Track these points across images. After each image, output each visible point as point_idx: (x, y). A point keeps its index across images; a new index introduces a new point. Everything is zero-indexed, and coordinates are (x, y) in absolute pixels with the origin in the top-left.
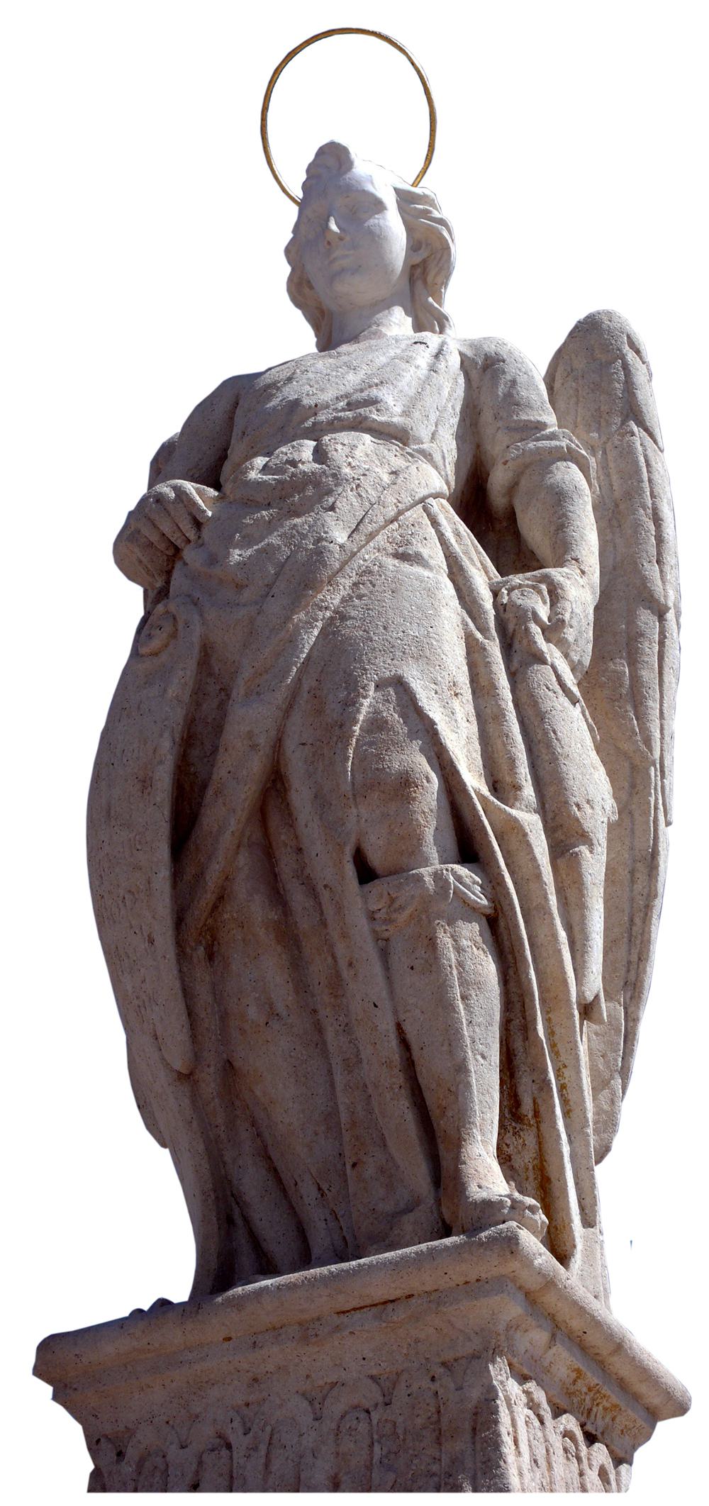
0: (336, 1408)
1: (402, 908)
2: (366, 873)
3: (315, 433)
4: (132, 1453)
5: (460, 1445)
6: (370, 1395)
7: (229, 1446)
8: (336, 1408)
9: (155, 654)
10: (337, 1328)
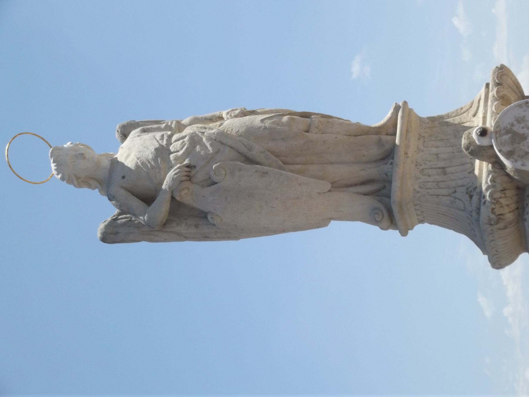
0: (421, 147)
1: (319, 126)
2: (307, 131)
3: (169, 143)
4: (418, 189)
5: (436, 123)
6: (422, 140)
7: (423, 169)
8: (421, 147)
9: (226, 174)
10: (409, 141)
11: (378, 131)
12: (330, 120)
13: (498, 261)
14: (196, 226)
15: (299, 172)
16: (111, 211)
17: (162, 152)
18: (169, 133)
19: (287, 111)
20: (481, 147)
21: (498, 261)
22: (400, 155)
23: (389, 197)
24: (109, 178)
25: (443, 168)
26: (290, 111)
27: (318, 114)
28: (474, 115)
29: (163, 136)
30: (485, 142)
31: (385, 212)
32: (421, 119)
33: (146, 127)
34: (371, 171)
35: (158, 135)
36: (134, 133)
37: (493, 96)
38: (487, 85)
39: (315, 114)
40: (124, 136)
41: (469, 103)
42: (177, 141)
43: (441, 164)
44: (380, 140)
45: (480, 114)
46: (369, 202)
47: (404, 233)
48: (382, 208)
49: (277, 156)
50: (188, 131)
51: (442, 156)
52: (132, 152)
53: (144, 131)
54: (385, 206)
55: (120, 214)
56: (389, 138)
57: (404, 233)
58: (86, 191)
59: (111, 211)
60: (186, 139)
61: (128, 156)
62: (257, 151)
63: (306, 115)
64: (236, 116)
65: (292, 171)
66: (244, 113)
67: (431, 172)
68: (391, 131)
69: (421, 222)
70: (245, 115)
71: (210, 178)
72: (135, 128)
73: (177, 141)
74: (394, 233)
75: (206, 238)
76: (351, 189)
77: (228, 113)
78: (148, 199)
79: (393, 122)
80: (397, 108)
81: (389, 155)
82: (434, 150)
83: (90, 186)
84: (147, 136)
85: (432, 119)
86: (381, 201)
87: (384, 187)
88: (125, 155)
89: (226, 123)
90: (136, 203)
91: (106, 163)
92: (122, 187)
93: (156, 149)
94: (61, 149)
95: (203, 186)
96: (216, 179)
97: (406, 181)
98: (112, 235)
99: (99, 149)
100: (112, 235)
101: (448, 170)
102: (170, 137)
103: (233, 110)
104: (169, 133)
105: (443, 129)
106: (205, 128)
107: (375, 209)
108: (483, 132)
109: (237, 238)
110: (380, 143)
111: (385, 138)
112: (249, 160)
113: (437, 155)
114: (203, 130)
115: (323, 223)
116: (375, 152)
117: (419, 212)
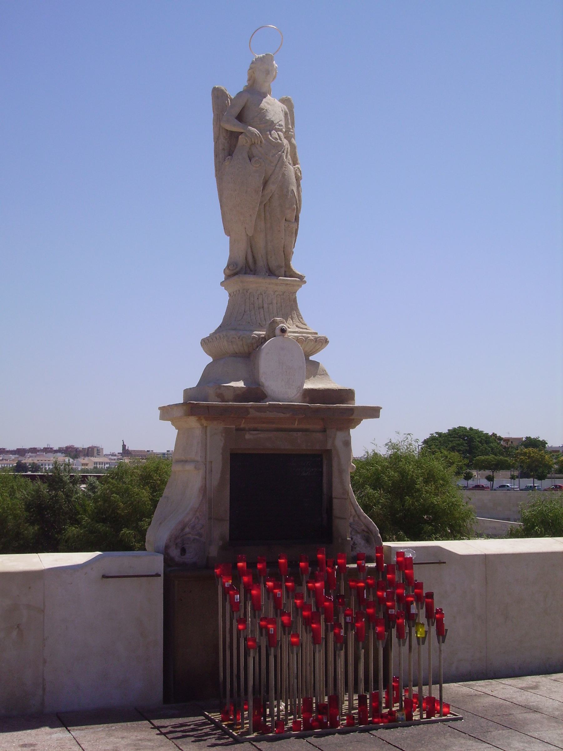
0: (277, 293)
4: (249, 292)
8: (277, 293)
11: (288, 266)
12: (294, 235)
13: (205, 343)
14: (223, 149)
15: (259, 215)
16: (232, 93)
17: (270, 126)
18: (284, 130)
19: (300, 206)
20: (274, 329)
21: (205, 343)
22: (273, 280)
23: (245, 273)
24: (255, 91)
25: (263, 307)
26: (300, 209)
27: (298, 227)
28: (297, 326)
29: (282, 126)
30: (278, 332)
31: (235, 271)
32: (295, 292)
33: (289, 115)
34: (261, 263)
35: (283, 123)
36: (285, 107)
37: (308, 337)
38: (317, 334)
39: (298, 225)
40: (283, 101)
41: (305, 323)
42: (278, 134)
43: (266, 306)
44: (282, 267)
45: (297, 330)
46: (241, 261)
47: (222, 284)
48: (237, 270)
49: (269, 200)
50: (285, 142)
51: (271, 306)
52: (273, 107)
53: (286, 114)
54: (237, 270)
55: (231, 99)
56: (283, 273)
57: (222, 284)
58: (246, 78)
59: (232, 93)
60: (279, 141)
61: (268, 103)
62: (272, 187)
63: (297, 219)
64: (296, 174)
65: (259, 211)
66: (298, 179)
67: (260, 299)
68: (287, 274)
69: (230, 295)
70: (296, 180)
71: (254, 157)
72: (288, 109)
73: (278, 134)
74: (222, 278)
75: (216, 156)
76: (249, 250)
77: (298, 168)
78: (240, 117)
79: (292, 274)
80: (301, 278)
81: (271, 273)
82: (275, 302)
83: (249, 80)
84: (282, 116)
85: (295, 300)
86: (242, 268)
87: (251, 271)
88: (269, 102)
89: (291, 167)
90: (237, 110)
91: (264, 90)
92: (247, 101)
93: (272, 122)
94: (272, 61)
95: (248, 152)
96: (253, 160)
97: (254, 283)
98: (218, 95)
99: (274, 85)
100: (218, 95)
101: (262, 310)
102: (281, 131)
103: (300, 172)
104: (284, 130)
105: (290, 308)
106: (287, 154)
107: (237, 265)
108: (283, 331)
109: (216, 175)
110: (280, 267)
111: (283, 270)
112: (265, 183)
113: (272, 303)
114: (285, 152)
115: (228, 231)
116: (273, 264)
117: (235, 293)
